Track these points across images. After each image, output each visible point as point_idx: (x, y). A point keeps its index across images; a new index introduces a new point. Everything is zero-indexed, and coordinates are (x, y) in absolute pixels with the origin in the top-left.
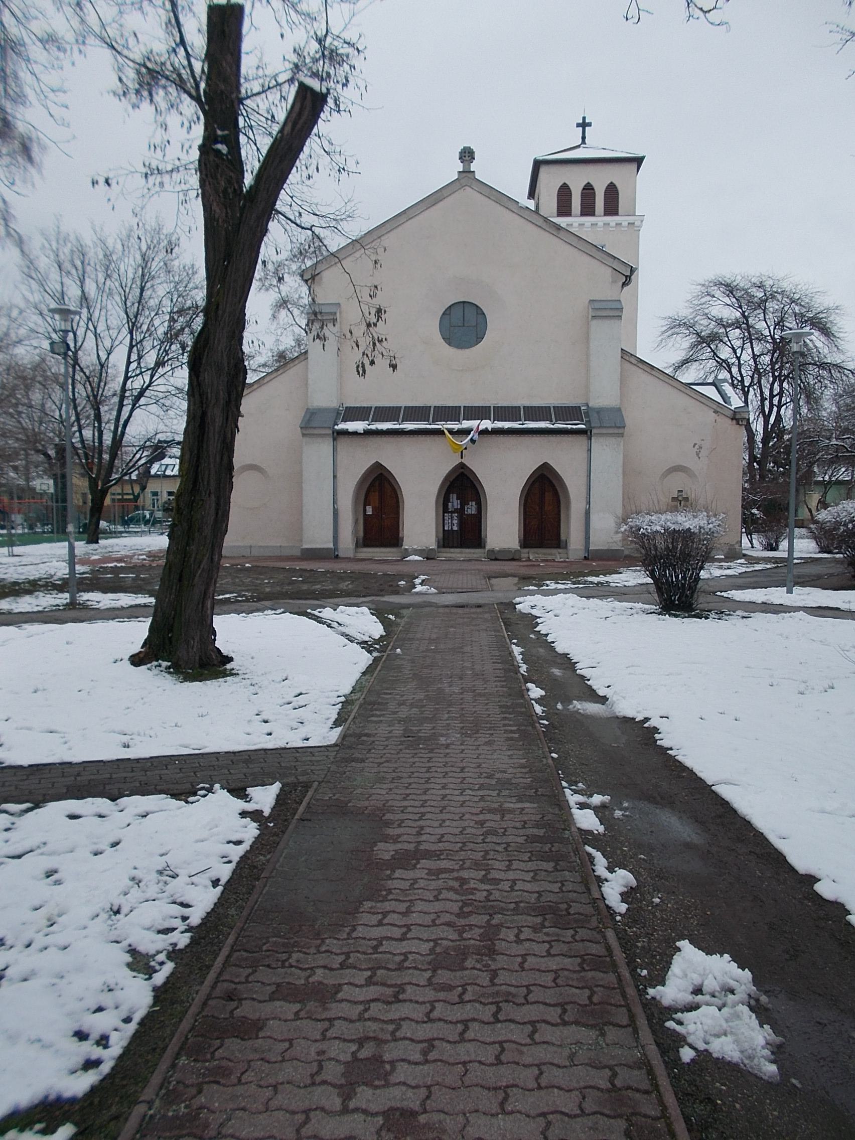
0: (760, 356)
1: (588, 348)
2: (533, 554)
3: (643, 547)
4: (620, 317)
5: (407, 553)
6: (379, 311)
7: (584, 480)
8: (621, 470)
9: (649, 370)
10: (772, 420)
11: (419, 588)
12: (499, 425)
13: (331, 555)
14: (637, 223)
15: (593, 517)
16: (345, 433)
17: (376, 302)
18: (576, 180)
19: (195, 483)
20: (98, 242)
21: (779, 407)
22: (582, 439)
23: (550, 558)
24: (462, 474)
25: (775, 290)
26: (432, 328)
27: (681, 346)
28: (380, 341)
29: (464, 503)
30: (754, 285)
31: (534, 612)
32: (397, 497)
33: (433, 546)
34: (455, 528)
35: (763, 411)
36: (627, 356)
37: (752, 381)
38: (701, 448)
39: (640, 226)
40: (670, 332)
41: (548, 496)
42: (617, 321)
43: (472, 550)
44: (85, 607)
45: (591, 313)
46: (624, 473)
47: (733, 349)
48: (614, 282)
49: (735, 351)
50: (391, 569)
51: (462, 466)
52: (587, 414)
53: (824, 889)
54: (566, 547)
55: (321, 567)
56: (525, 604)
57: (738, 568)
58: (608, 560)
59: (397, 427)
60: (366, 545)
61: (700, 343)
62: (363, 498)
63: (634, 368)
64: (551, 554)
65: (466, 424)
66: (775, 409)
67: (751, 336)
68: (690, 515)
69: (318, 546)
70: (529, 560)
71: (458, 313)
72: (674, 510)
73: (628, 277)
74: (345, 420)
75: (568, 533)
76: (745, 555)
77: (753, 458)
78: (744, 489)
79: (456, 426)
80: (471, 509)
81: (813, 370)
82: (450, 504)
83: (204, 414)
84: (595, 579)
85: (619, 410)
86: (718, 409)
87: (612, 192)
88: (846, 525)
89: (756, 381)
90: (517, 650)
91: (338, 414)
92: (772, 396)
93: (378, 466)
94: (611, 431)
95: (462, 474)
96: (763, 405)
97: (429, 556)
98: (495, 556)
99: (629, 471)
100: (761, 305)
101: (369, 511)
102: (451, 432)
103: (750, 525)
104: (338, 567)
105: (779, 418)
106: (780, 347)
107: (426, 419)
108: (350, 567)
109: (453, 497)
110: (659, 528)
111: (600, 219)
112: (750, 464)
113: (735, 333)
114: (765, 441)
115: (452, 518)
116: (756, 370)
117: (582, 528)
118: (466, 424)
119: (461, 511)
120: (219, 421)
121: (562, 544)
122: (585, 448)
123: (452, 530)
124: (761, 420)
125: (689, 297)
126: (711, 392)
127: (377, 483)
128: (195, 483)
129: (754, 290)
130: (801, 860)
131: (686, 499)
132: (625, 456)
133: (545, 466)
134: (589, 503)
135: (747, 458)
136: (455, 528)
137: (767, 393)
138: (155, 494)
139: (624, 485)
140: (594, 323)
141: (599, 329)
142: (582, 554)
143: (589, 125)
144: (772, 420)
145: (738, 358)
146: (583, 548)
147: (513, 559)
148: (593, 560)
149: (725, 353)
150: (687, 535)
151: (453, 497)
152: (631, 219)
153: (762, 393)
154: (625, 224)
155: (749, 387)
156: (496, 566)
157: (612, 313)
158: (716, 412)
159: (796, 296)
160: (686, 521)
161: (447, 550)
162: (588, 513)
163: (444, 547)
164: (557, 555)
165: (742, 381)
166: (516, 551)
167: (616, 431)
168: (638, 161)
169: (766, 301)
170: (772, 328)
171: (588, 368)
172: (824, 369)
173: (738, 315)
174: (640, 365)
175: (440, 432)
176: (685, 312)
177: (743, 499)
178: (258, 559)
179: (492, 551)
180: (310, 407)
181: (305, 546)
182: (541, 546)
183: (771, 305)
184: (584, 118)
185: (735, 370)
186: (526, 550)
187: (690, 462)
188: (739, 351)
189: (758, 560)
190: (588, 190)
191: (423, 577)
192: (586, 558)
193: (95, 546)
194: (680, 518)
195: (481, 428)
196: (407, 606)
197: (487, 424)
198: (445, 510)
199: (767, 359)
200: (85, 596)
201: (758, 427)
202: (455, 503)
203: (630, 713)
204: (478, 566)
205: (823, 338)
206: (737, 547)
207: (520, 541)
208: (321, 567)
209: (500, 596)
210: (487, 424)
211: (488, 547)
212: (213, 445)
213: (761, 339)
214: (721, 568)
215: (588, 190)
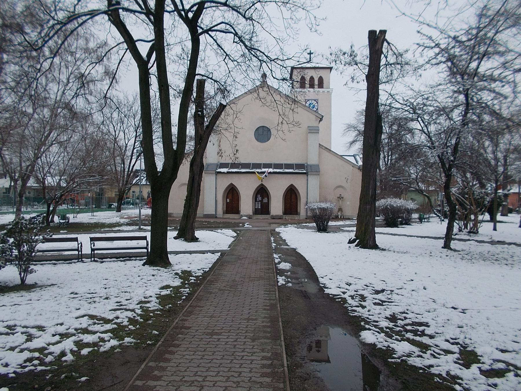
1: (307, 143)
2: (287, 217)
4: (318, 133)
5: (242, 216)
6: (237, 151)
7: (306, 190)
8: (318, 187)
11: (246, 226)
12: (275, 170)
13: (214, 216)
16: (220, 173)
17: (236, 148)
18: (308, 74)
19: (191, 194)
20: (125, 98)
22: (305, 176)
23: (293, 218)
24: (262, 188)
26: (251, 135)
28: (237, 158)
31: (280, 231)
33: (251, 214)
34: (259, 207)
39: (332, 93)
40: (348, 130)
41: (293, 196)
42: (317, 134)
44: (142, 229)
48: (316, 120)
50: (237, 221)
51: (262, 185)
52: (307, 167)
54: (299, 215)
55: (212, 220)
56: (277, 230)
59: (239, 171)
60: (227, 213)
62: (226, 196)
65: (263, 170)
69: (210, 213)
70: (286, 219)
71: (261, 130)
74: (220, 168)
79: (260, 171)
80: (265, 200)
83: (194, 177)
84: (304, 224)
85: (318, 166)
86: (353, 165)
87: (321, 80)
90: (272, 239)
91: (218, 166)
93: (232, 184)
95: (291, 188)
97: (250, 217)
98: (273, 218)
99: (321, 187)
101: (228, 201)
102: (258, 172)
104: (218, 220)
107: (249, 168)
108: (222, 221)
109: (259, 196)
111: (317, 89)
118: (263, 170)
119: (261, 201)
120: (197, 179)
121: (298, 214)
122: (306, 179)
127: (231, 191)
128: (191, 194)
131: (343, 198)
132: (320, 181)
133: (292, 185)
134: (307, 198)
136: (259, 207)
138: (133, 192)
139: (320, 192)
140: (309, 135)
141: (312, 137)
142: (305, 217)
143: (312, 53)
146: (305, 215)
147: (280, 219)
150: (324, 209)
151: (259, 196)
152: (328, 90)
154: (326, 91)
156: (273, 221)
157: (315, 131)
158: (353, 166)
160: (324, 205)
163: (255, 214)
164: (296, 217)
166: (281, 216)
167: (317, 173)
175: (254, 173)
179: (272, 216)
180: (207, 162)
181: (205, 213)
182: (291, 214)
184: (310, 51)
187: (344, 184)
190: (312, 79)
191: (247, 223)
192: (306, 218)
193: (119, 213)
194: (322, 204)
195: (269, 171)
196: (243, 230)
197: (271, 170)
198: (256, 201)
200: (142, 227)
202: (259, 198)
203: (293, 247)
204: (268, 221)
207: (283, 212)
208: (212, 220)
209: (272, 228)
210: (271, 170)
211: (271, 214)
212: (196, 185)
215: (312, 79)
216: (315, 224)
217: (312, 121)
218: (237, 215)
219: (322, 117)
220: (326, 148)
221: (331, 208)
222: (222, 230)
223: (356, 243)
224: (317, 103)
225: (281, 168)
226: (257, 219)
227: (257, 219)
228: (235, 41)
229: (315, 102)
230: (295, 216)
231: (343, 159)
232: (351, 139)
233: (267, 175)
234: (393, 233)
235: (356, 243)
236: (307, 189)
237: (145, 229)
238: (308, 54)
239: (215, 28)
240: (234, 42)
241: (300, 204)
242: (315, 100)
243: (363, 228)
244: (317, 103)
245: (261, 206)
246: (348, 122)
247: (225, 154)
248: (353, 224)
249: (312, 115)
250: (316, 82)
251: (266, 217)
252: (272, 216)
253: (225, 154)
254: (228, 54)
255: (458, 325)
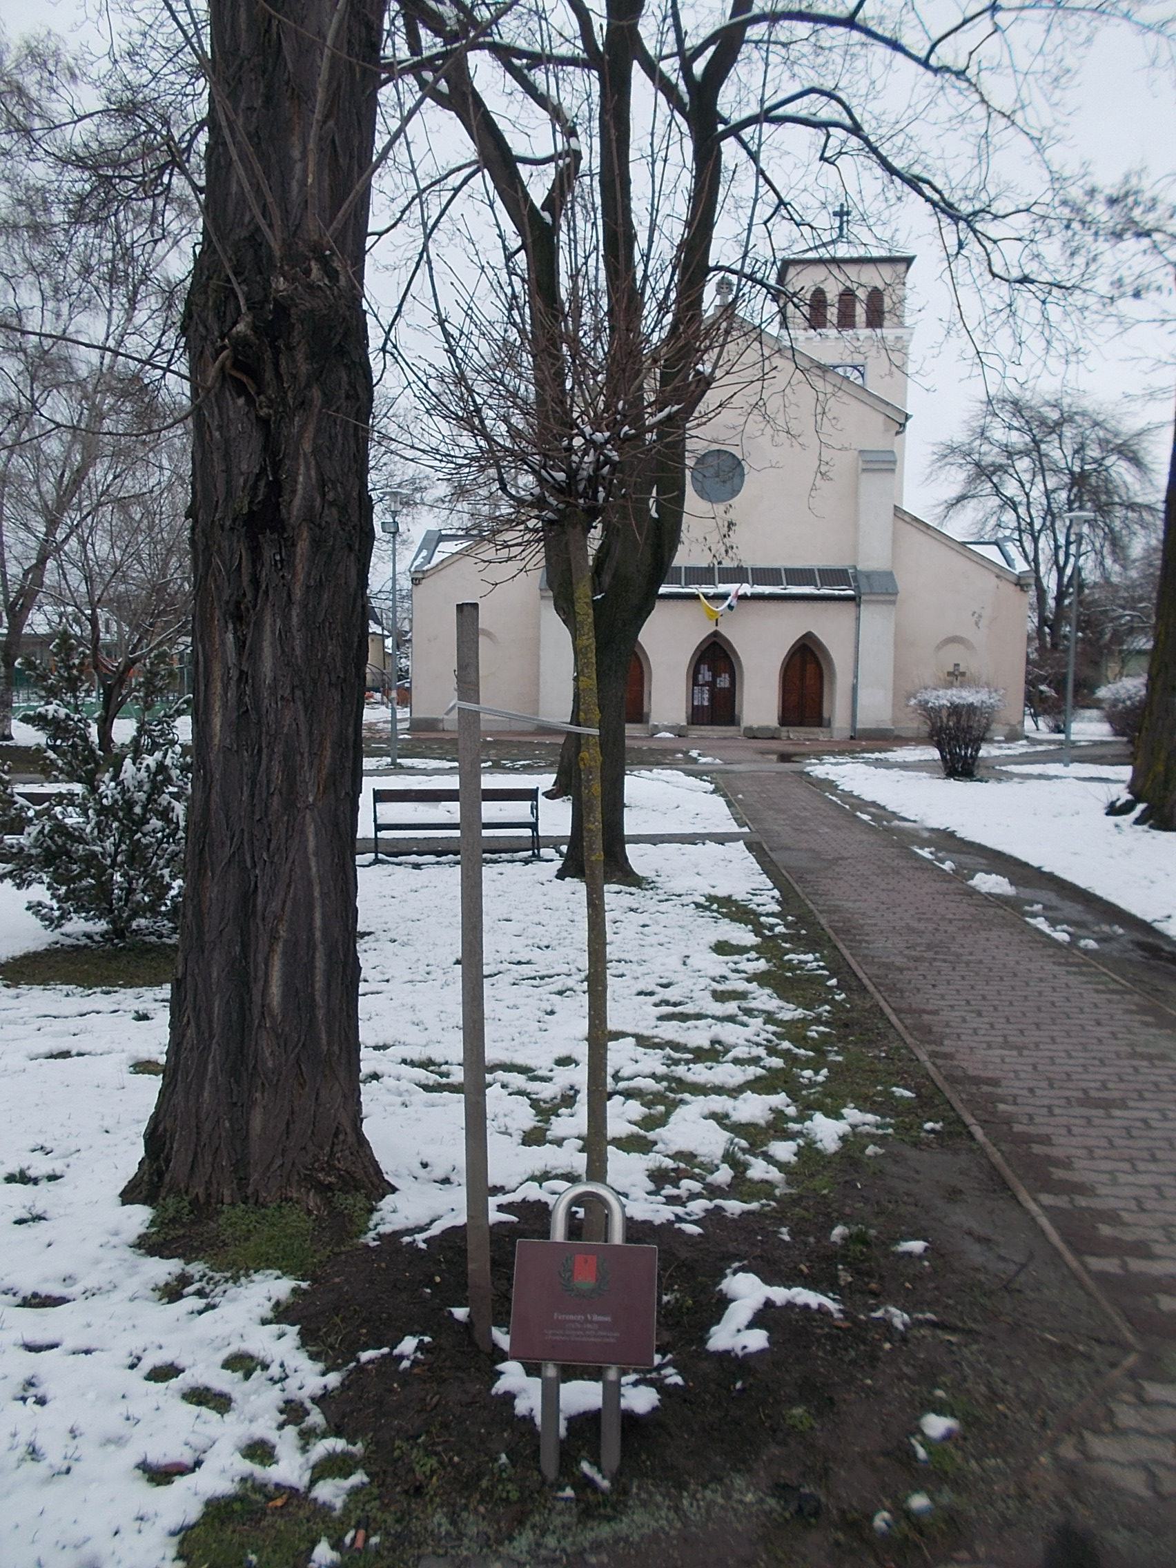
0: (1054, 491)
1: (857, 504)
2: (795, 733)
3: (930, 719)
4: (893, 470)
5: (656, 729)
7: (851, 650)
9: (924, 529)
10: (1068, 571)
14: (905, 338)
15: (860, 692)
17: (729, 517)
21: (1078, 556)
22: (850, 606)
23: (812, 737)
24: (715, 643)
25: (1074, 410)
27: (955, 479)
29: (715, 676)
30: (1048, 404)
32: (641, 667)
34: (706, 703)
35: (1056, 562)
36: (897, 510)
37: (1044, 524)
38: (980, 616)
41: (810, 668)
43: (724, 728)
44: (401, 766)
45: (861, 465)
46: (896, 645)
47: (1020, 482)
48: (887, 430)
49: (1023, 486)
51: (716, 634)
52: (855, 579)
53: (1046, 869)
54: (829, 725)
57: (1020, 748)
58: (877, 740)
61: (978, 476)
63: (909, 527)
64: (813, 733)
65: (722, 588)
66: (1072, 560)
67: (1041, 469)
68: (973, 691)
70: (789, 738)
72: (950, 685)
73: (900, 422)
75: (832, 711)
76: (1027, 738)
77: (1043, 621)
78: (1028, 662)
79: (711, 591)
80: (723, 682)
81: (1119, 512)
82: (700, 676)
86: (1000, 574)
87: (876, 296)
88: (1124, 702)
89: (1048, 524)
92: (1068, 543)
94: (881, 598)
95: (715, 643)
96: (1056, 555)
97: (680, 733)
98: (753, 734)
99: (901, 643)
100: (1055, 428)
102: (706, 596)
103: (1036, 703)
105: (1077, 570)
106: (1078, 480)
109: (704, 668)
110: (945, 702)
112: (1039, 630)
113: (1023, 464)
114: (1059, 598)
115: (702, 692)
116: (1049, 510)
117: (848, 700)
118: (722, 588)
119: (712, 685)
121: (825, 723)
122: (853, 615)
123: (703, 706)
124: (1054, 574)
125: (966, 416)
126: (992, 553)
129: (1048, 409)
130: (1035, 864)
131: (963, 674)
132: (897, 625)
133: (809, 636)
134: (856, 677)
135: (1036, 620)
136: (706, 703)
137: (1062, 541)
139: (895, 657)
140: (864, 476)
141: (871, 485)
142: (848, 734)
144: (1068, 571)
145: (1027, 495)
146: (849, 727)
147: (773, 738)
148: (861, 739)
149: (1011, 489)
150: (955, 710)
151: (704, 668)
152: (899, 332)
153: (1055, 540)
155: (1040, 531)
158: (998, 577)
159: (1100, 418)
160: (969, 696)
161: (697, 727)
162: (855, 688)
163: (693, 724)
164: (820, 734)
165: (1031, 524)
167: (887, 598)
168: (908, 261)
169: (1062, 424)
170: (1069, 459)
171: (856, 526)
172: (1133, 511)
173: (1028, 439)
174: (914, 523)
175: (694, 597)
176: (960, 436)
177: (1028, 673)
178: (499, 732)
179: (750, 729)
182: (801, 724)
183: (1068, 431)
185: (1022, 510)
186: (784, 729)
187: (968, 633)
188: (1027, 486)
189: (1041, 742)
190: (847, 296)
192: (852, 738)
194: (964, 693)
195: (741, 592)
197: (746, 589)
199: (1063, 495)
200: (399, 761)
201: (1051, 582)
202: (706, 675)
203: (936, 826)
205: (1134, 470)
206: (1018, 727)
210: (746, 589)
213: (1057, 471)
214: (1000, 748)
216: (936, 754)
217: (874, 437)
218: (639, 726)
219: (907, 417)
220: (916, 519)
221: (992, 707)
222: (651, 771)
223: (1136, 813)
224: (862, 375)
225: (777, 583)
226: (702, 738)
227: (702, 738)
228: (827, 155)
229: (857, 374)
230: (816, 730)
231: (967, 554)
232: (954, 491)
233: (734, 603)
234: (1043, 781)
235: (1136, 813)
236: (857, 647)
237: (413, 768)
238: (835, 214)
239: (788, 110)
240: (822, 158)
241: (832, 690)
242: (855, 367)
243: (1160, 768)
244: (862, 375)
245: (711, 699)
246: (945, 437)
247: (689, 535)
248: (1015, 756)
249: (875, 414)
250: (860, 311)
251: (729, 734)
252: (746, 729)
253: (689, 535)
254: (786, 200)
255: (137, 1012)
